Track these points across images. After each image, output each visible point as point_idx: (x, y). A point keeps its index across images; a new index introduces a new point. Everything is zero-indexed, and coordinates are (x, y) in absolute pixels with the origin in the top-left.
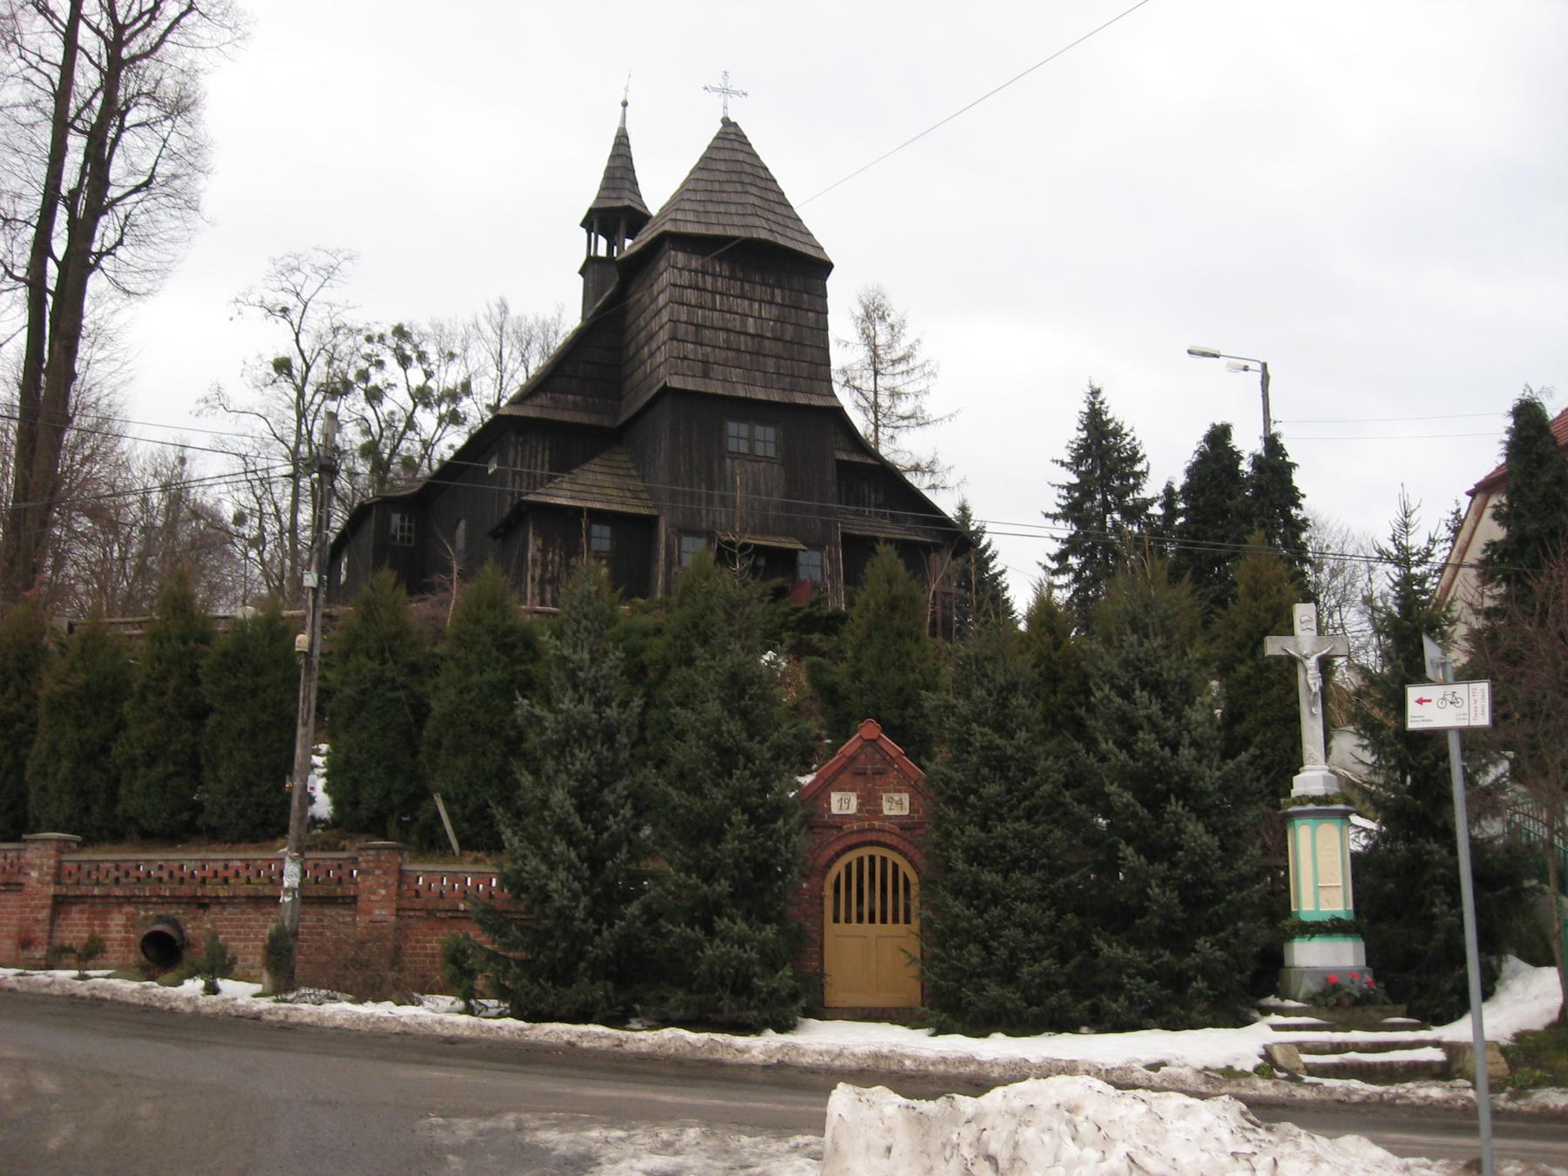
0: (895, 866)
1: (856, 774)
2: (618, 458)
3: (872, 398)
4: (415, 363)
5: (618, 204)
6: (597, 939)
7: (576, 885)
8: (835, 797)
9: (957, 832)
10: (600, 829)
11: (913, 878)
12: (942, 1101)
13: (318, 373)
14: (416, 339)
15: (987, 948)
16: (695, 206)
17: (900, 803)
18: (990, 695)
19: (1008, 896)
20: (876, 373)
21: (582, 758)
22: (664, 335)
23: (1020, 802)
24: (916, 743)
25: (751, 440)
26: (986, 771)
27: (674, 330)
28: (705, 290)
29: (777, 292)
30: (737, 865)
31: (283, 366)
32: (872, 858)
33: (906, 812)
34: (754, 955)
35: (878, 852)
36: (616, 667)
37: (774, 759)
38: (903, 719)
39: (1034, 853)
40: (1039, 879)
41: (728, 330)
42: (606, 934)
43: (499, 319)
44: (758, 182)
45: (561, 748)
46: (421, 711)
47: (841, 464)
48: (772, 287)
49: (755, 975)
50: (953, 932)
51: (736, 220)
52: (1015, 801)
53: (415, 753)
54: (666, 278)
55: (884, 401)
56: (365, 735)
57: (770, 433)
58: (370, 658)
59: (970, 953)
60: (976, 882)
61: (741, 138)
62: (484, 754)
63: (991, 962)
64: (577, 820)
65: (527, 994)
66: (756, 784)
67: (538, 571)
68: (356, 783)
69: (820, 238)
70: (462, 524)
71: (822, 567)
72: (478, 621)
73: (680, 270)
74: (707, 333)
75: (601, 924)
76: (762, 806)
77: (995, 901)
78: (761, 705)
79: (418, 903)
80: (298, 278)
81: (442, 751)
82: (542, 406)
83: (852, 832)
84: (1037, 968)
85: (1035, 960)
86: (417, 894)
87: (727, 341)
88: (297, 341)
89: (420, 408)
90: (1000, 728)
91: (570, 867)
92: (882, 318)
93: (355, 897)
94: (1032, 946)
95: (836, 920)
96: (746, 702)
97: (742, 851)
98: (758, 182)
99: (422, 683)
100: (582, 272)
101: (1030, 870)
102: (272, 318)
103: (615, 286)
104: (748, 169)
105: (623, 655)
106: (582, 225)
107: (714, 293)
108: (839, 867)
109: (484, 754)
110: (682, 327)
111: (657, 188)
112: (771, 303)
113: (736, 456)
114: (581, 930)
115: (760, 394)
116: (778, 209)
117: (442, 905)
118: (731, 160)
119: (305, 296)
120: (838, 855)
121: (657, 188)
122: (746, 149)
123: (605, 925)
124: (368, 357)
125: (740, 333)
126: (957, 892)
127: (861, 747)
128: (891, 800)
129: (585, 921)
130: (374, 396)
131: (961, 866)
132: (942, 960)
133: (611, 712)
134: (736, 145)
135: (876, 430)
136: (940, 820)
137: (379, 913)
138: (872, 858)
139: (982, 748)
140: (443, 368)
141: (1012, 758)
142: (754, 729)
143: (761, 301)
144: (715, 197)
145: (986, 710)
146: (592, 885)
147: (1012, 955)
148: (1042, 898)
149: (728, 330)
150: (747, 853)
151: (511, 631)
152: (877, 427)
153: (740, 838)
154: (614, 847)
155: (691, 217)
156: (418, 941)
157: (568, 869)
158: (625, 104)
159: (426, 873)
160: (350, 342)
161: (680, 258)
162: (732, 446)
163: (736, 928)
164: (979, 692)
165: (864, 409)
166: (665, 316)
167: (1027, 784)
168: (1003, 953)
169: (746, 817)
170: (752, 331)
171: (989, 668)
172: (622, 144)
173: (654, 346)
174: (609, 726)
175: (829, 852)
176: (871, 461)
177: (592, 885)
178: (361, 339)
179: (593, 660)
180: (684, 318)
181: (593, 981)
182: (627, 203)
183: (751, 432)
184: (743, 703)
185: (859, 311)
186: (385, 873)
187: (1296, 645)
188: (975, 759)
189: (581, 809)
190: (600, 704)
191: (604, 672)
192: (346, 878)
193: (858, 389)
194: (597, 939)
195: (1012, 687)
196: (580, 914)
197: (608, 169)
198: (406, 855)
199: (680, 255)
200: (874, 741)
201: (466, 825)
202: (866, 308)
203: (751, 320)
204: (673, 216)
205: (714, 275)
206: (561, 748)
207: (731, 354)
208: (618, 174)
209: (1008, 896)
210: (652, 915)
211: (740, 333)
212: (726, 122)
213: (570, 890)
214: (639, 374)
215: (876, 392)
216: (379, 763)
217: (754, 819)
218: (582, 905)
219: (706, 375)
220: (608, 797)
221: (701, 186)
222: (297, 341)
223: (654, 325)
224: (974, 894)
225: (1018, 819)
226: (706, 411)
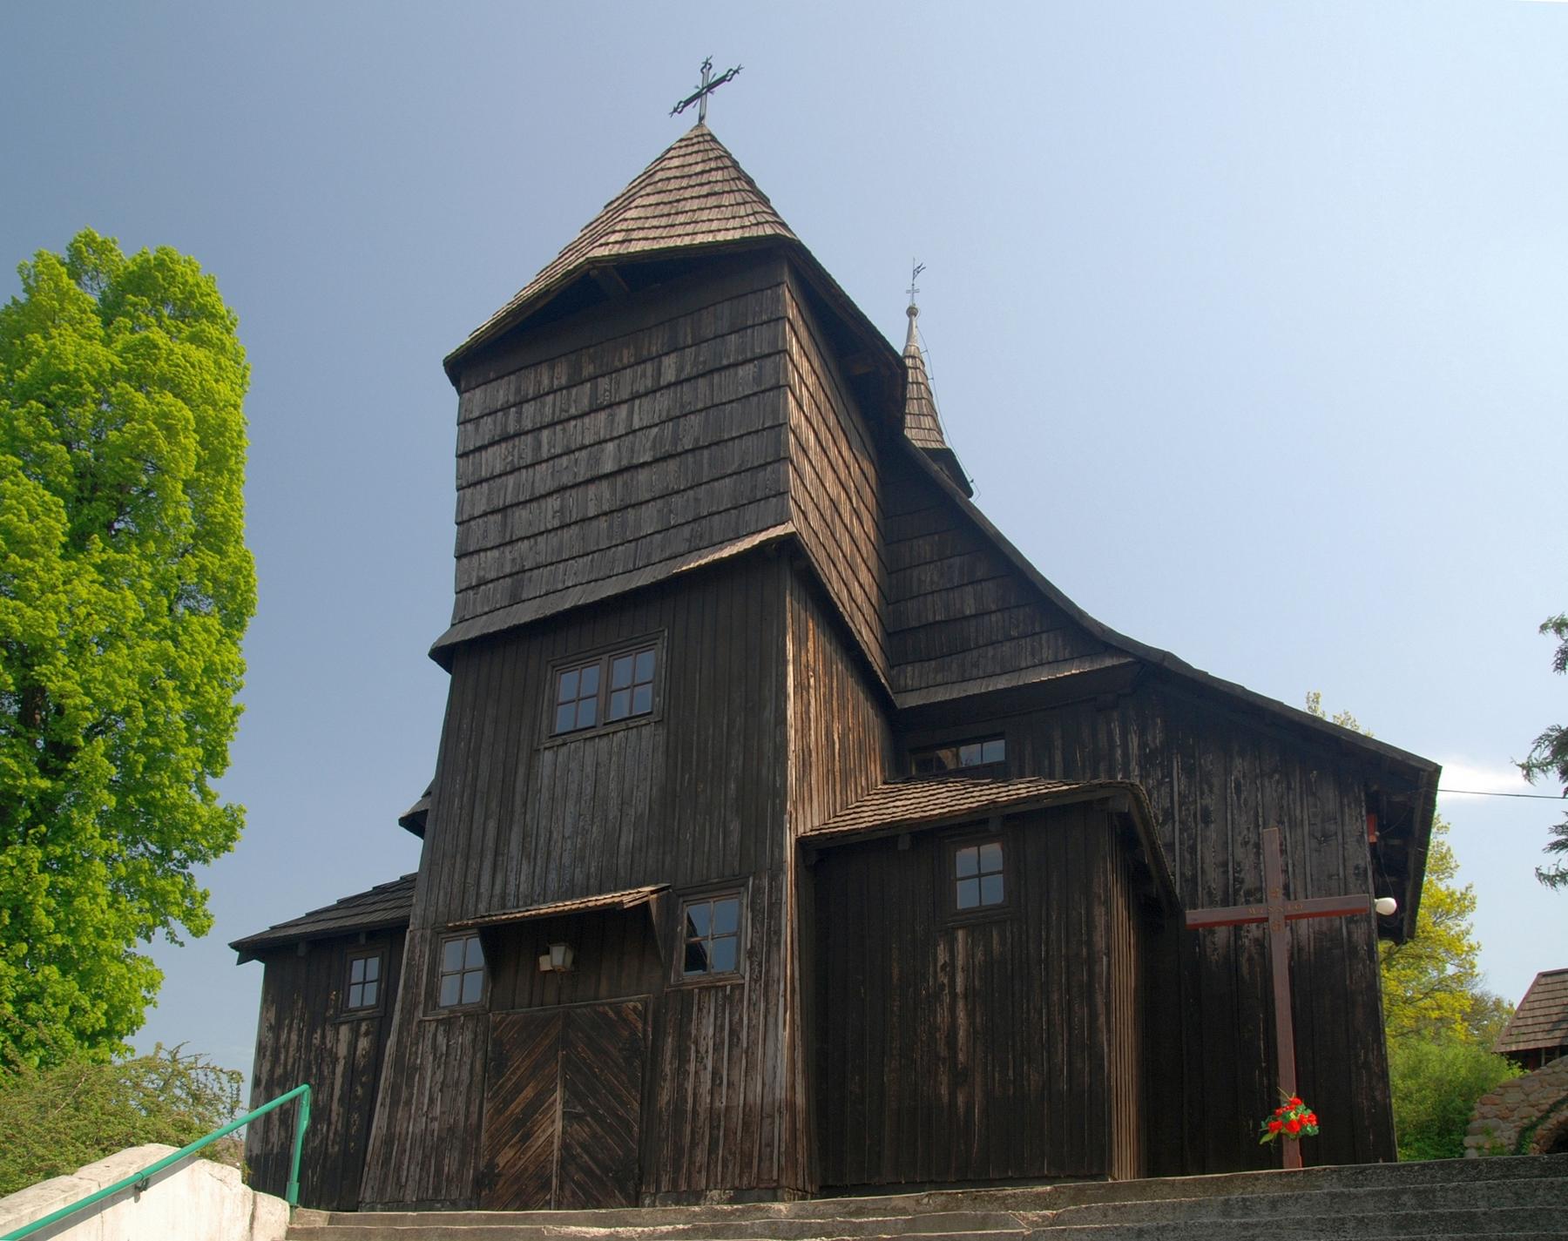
158: (912, 312)
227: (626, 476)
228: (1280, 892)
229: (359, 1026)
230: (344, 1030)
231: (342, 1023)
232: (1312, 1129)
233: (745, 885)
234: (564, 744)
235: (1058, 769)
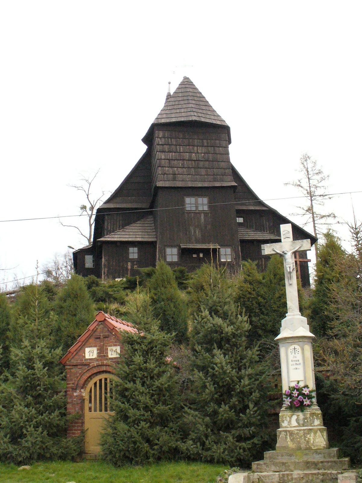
2: (148, 220)
8: (87, 350)
32: (106, 379)
44: (196, 99)
57: (205, 200)
67: (106, 269)
69: (223, 117)
87: (183, 164)
88: (88, 198)
98: (196, 99)
112: (203, 146)
120: (90, 377)
128: (112, 350)
138: (106, 379)
144: (175, 107)
158: (169, 83)
176: (264, 209)
187: (281, 247)
222: (88, 198)
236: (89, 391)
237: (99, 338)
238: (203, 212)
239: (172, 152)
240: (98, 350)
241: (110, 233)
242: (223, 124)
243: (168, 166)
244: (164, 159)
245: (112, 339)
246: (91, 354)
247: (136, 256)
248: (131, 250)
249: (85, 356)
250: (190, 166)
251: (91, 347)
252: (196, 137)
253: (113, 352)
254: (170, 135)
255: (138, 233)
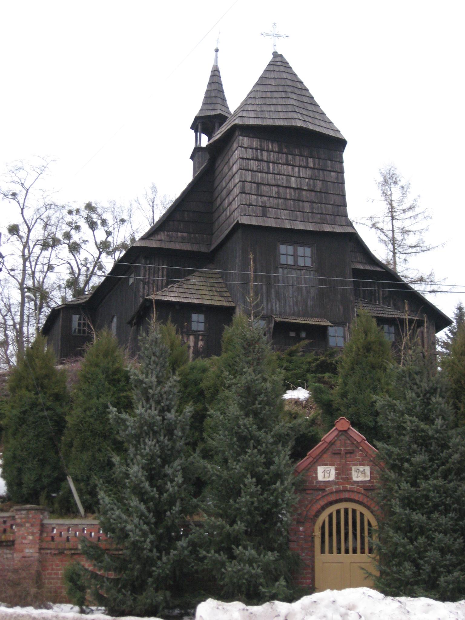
0: (362, 515)
1: (335, 454)
3: (390, 235)
4: (100, 226)
5: (213, 113)
6: (159, 563)
7: (145, 527)
8: (320, 470)
9: (396, 487)
10: (161, 490)
11: (374, 523)
12: (266, 605)
13: (38, 233)
14: (99, 211)
15: (418, 566)
16: (254, 108)
17: (364, 472)
18: (419, 396)
19: (430, 530)
20: (393, 218)
21: (150, 445)
22: (237, 191)
23: (439, 467)
24: (373, 433)
25: (295, 256)
26: (415, 446)
27: (243, 187)
28: (262, 160)
29: (310, 160)
30: (250, 513)
31: (14, 230)
32: (346, 511)
33: (368, 479)
34: (259, 571)
35: (350, 506)
36: (174, 386)
37: (275, 443)
38: (376, 422)
39: (448, 501)
40: (452, 519)
41: (278, 186)
42: (164, 559)
43: (151, 196)
44: (296, 91)
45: (138, 438)
46: (60, 424)
47: (357, 273)
48: (307, 157)
49: (261, 584)
50: (394, 555)
51: (282, 115)
52: (435, 466)
53: (57, 453)
54: (236, 155)
55: (398, 236)
56: (25, 440)
57: (308, 251)
58: (29, 391)
59: (405, 568)
60: (409, 521)
61: (285, 64)
62: (100, 450)
63: (419, 574)
64: (147, 485)
65: (115, 599)
66: (262, 459)
68: (20, 470)
69: (337, 124)
70: (115, 320)
71: (344, 337)
72: (97, 365)
73: (246, 148)
74: (265, 188)
75: (161, 552)
76: (267, 474)
77: (422, 531)
78: (267, 407)
79: (53, 545)
80: (21, 174)
81: (73, 449)
82: (161, 240)
83: (332, 493)
84: (450, 578)
85: (449, 572)
86: (53, 539)
87: (278, 193)
88: (22, 213)
89: (104, 255)
90: (426, 418)
91: (141, 516)
92: (395, 183)
93: (13, 541)
94: (447, 563)
95: (323, 552)
96: (257, 405)
97: (253, 503)
98: (296, 91)
99: (61, 406)
100: (192, 157)
101: (446, 512)
102: (7, 200)
103: (209, 162)
104: (289, 83)
105: (178, 379)
106: (192, 128)
107: (268, 162)
108: (324, 516)
109: (100, 450)
110: (248, 185)
111: (235, 97)
112: (306, 167)
113: (286, 266)
114: (148, 556)
115: (300, 226)
116: (310, 107)
117: (68, 545)
118: (279, 77)
119: (27, 185)
120: (323, 508)
121: (235, 97)
122: (289, 70)
123: (164, 553)
124: (70, 224)
125: (286, 187)
126: (397, 529)
127: (337, 436)
128: (357, 471)
129: (151, 551)
130: (74, 248)
131: (398, 510)
132: (387, 574)
133: (171, 416)
134: (282, 69)
135: (394, 256)
136: (385, 480)
137: (28, 551)
138: (346, 511)
139: (413, 431)
140: (116, 229)
141: (432, 437)
142: (262, 424)
143: (300, 166)
144: (268, 101)
145: (415, 406)
146: (156, 527)
147: (434, 570)
148: (455, 531)
149: (278, 186)
150: (256, 504)
151: (118, 371)
152: (394, 253)
153: (252, 495)
154: (171, 503)
155: (252, 114)
156: (52, 569)
157: (140, 517)
158: (217, 50)
159: (57, 524)
160: (58, 214)
161: (246, 141)
162: (283, 260)
163: (247, 553)
164: (410, 395)
165: (385, 242)
166: (237, 179)
167: (444, 455)
168: (428, 568)
169: (254, 480)
170: (294, 185)
171: (417, 378)
172: (215, 74)
173: (231, 198)
174: (170, 424)
175: (317, 507)
176: (379, 269)
177: (156, 527)
178: (65, 212)
179: (159, 383)
180: (249, 179)
181: (157, 590)
182: (219, 112)
183: (295, 251)
184: (254, 406)
185: (381, 179)
186: (32, 525)
188: (407, 438)
189: (151, 478)
190: (162, 411)
191: (166, 389)
192: (8, 529)
193: (381, 230)
194: (159, 563)
195: (433, 391)
196: (147, 545)
197: (207, 91)
198: (46, 514)
199: (246, 139)
200: (345, 431)
201: (88, 497)
202: (385, 176)
203: (293, 179)
204: (240, 115)
205: (268, 151)
206: (138, 438)
207: (280, 201)
208: (213, 95)
209: (430, 530)
210: (194, 546)
211: (286, 187)
212: (275, 54)
213: (141, 530)
214: (223, 217)
215: (393, 231)
216: (34, 458)
217: (259, 481)
218: (148, 540)
219: (264, 215)
220: (168, 470)
221: (259, 95)
222: (22, 213)
223: (231, 185)
224: (409, 530)
225: (437, 478)
226: (266, 238)
227: (299, 191)
228: (133, 310)
229: (198, 337)
230: (192, 338)
231: (191, 335)
232: (160, 463)
233: (346, 325)
234: (286, 268)
235: (362, 296)
236: (321, 524)
237: (340, 454)
238: (305, 268)
239: (263, 172)
240: (336, 469)
241: (162, 288)
242: (339, 136)
243: (256, 193)
244: (250, 182)
245: (358, 455)
246: (327, 475)
247: (201, 327)
248: (194, 317)
249: (317, 478)
250: (288, 197)
251: (326, 465)
252: (297, 152)
253: (360, 473)
254: (261, 146)
255: (204, 292)
